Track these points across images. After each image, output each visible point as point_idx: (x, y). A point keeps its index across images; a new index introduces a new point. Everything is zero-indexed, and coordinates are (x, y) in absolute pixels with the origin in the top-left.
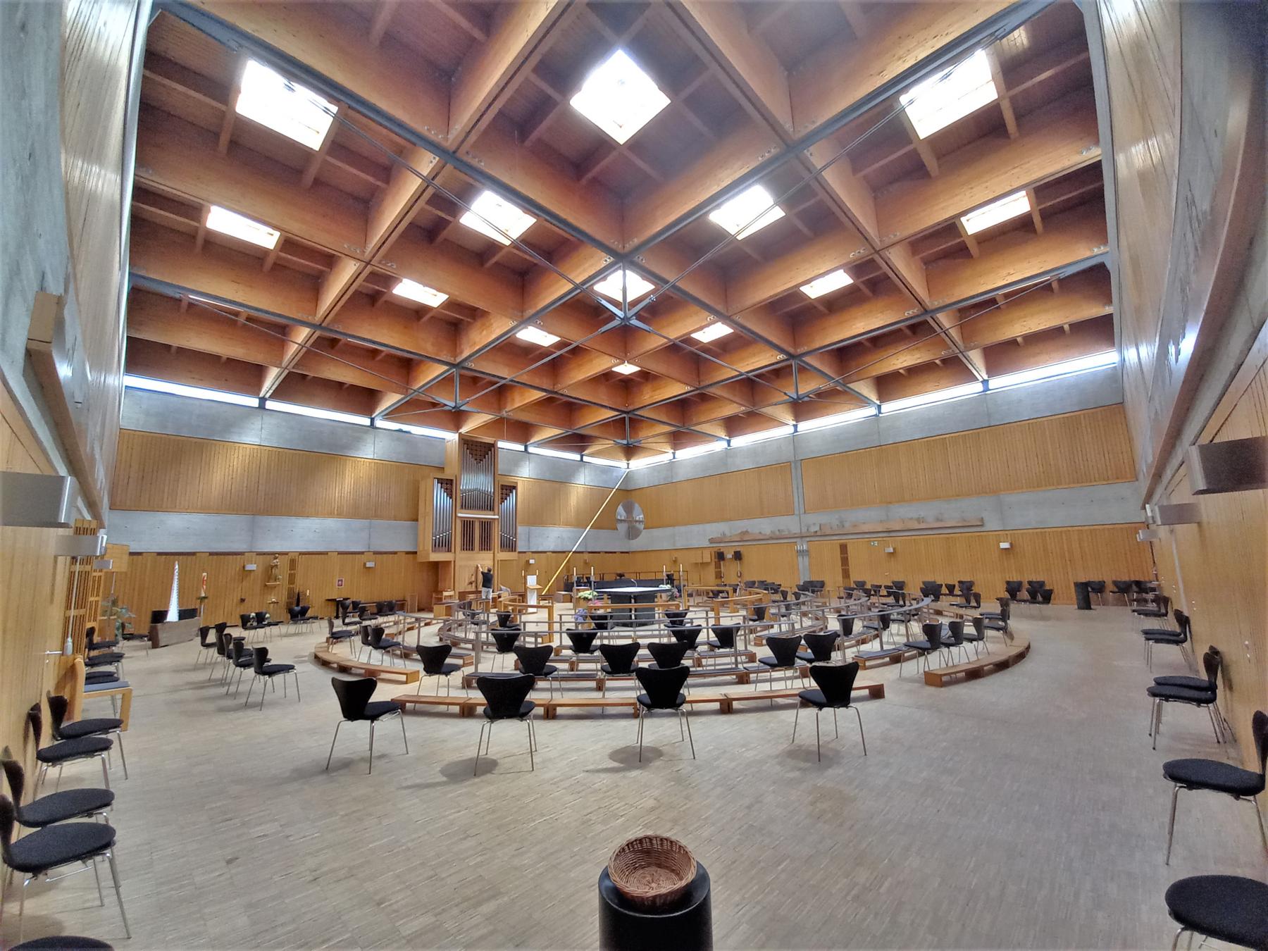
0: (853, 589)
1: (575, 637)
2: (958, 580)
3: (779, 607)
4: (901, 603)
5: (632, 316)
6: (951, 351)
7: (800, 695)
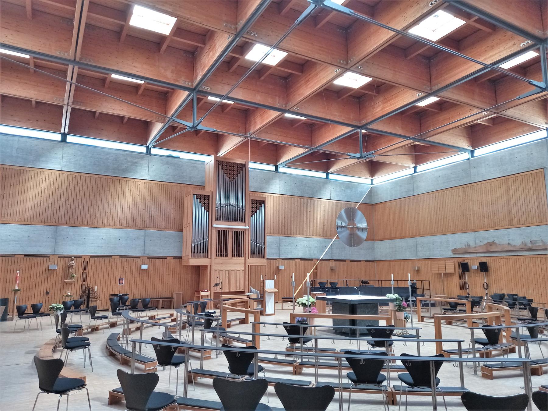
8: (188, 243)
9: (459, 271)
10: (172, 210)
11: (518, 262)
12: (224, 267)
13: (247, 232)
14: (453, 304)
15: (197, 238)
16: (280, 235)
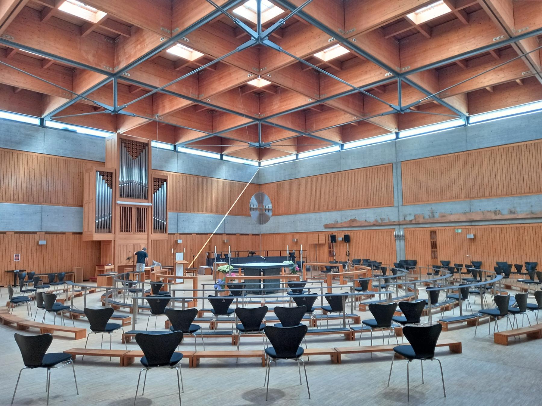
0: (439, 267)
1: (213, 301)
2: (526, 261)
3: (379, 281)
4: (478, 279)
5: (265, 37)
6: (529, 72)
7: (394, 350)
10: (70, 186)
12: (128, 242)
13: (150, 209)
14: (329, 268)
15: (100, 214)
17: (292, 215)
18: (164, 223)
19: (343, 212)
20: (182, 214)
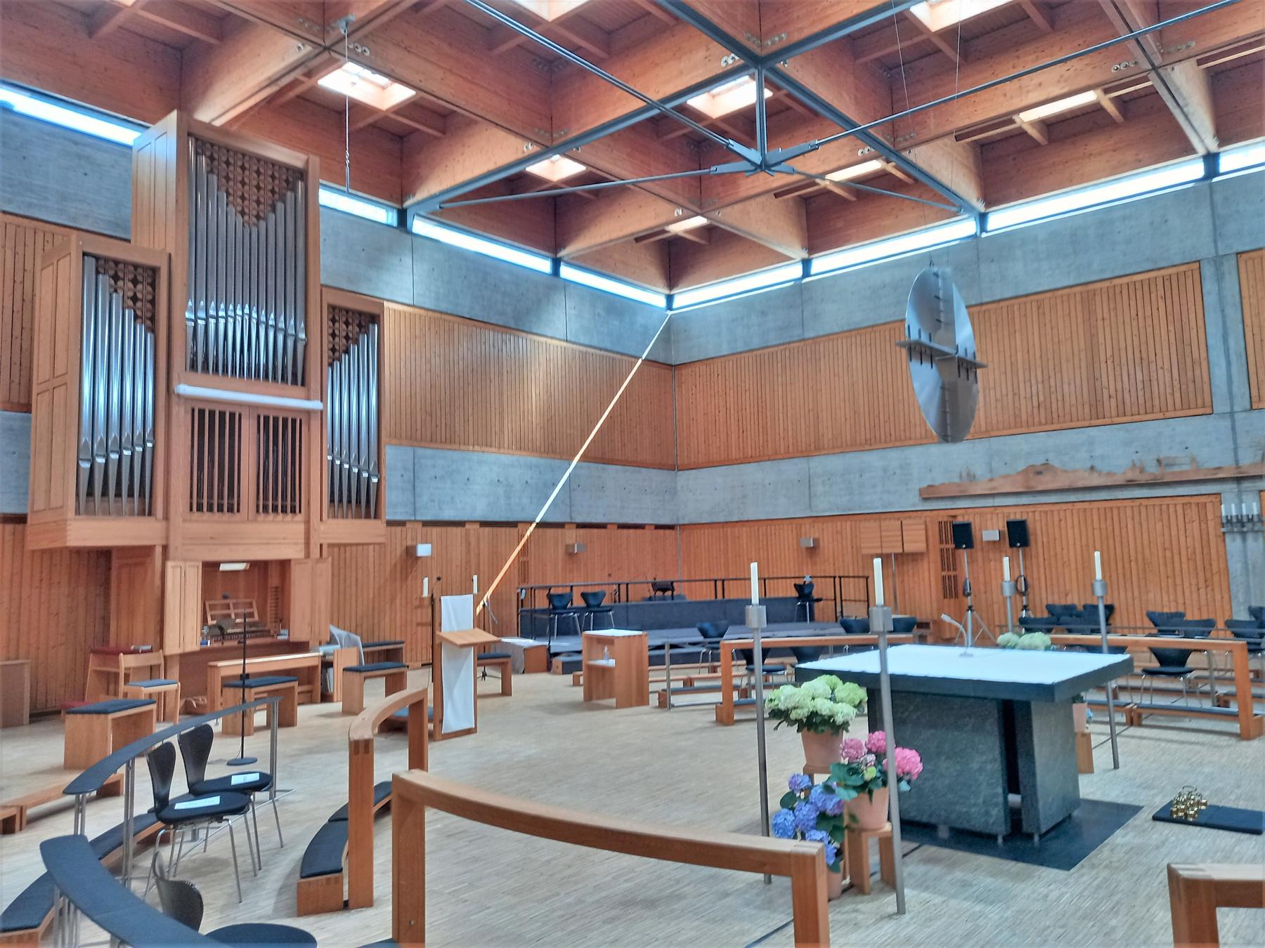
8: (57, 457)
9: (944, 546)
11: (1116, 518)
13: (315, 424)
16: (415, 444)
17: (795, 460)
18: (369, 479)
19: (995, 443)
20: (429, 452)
